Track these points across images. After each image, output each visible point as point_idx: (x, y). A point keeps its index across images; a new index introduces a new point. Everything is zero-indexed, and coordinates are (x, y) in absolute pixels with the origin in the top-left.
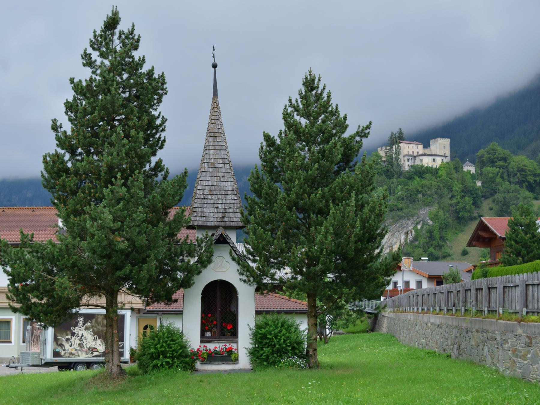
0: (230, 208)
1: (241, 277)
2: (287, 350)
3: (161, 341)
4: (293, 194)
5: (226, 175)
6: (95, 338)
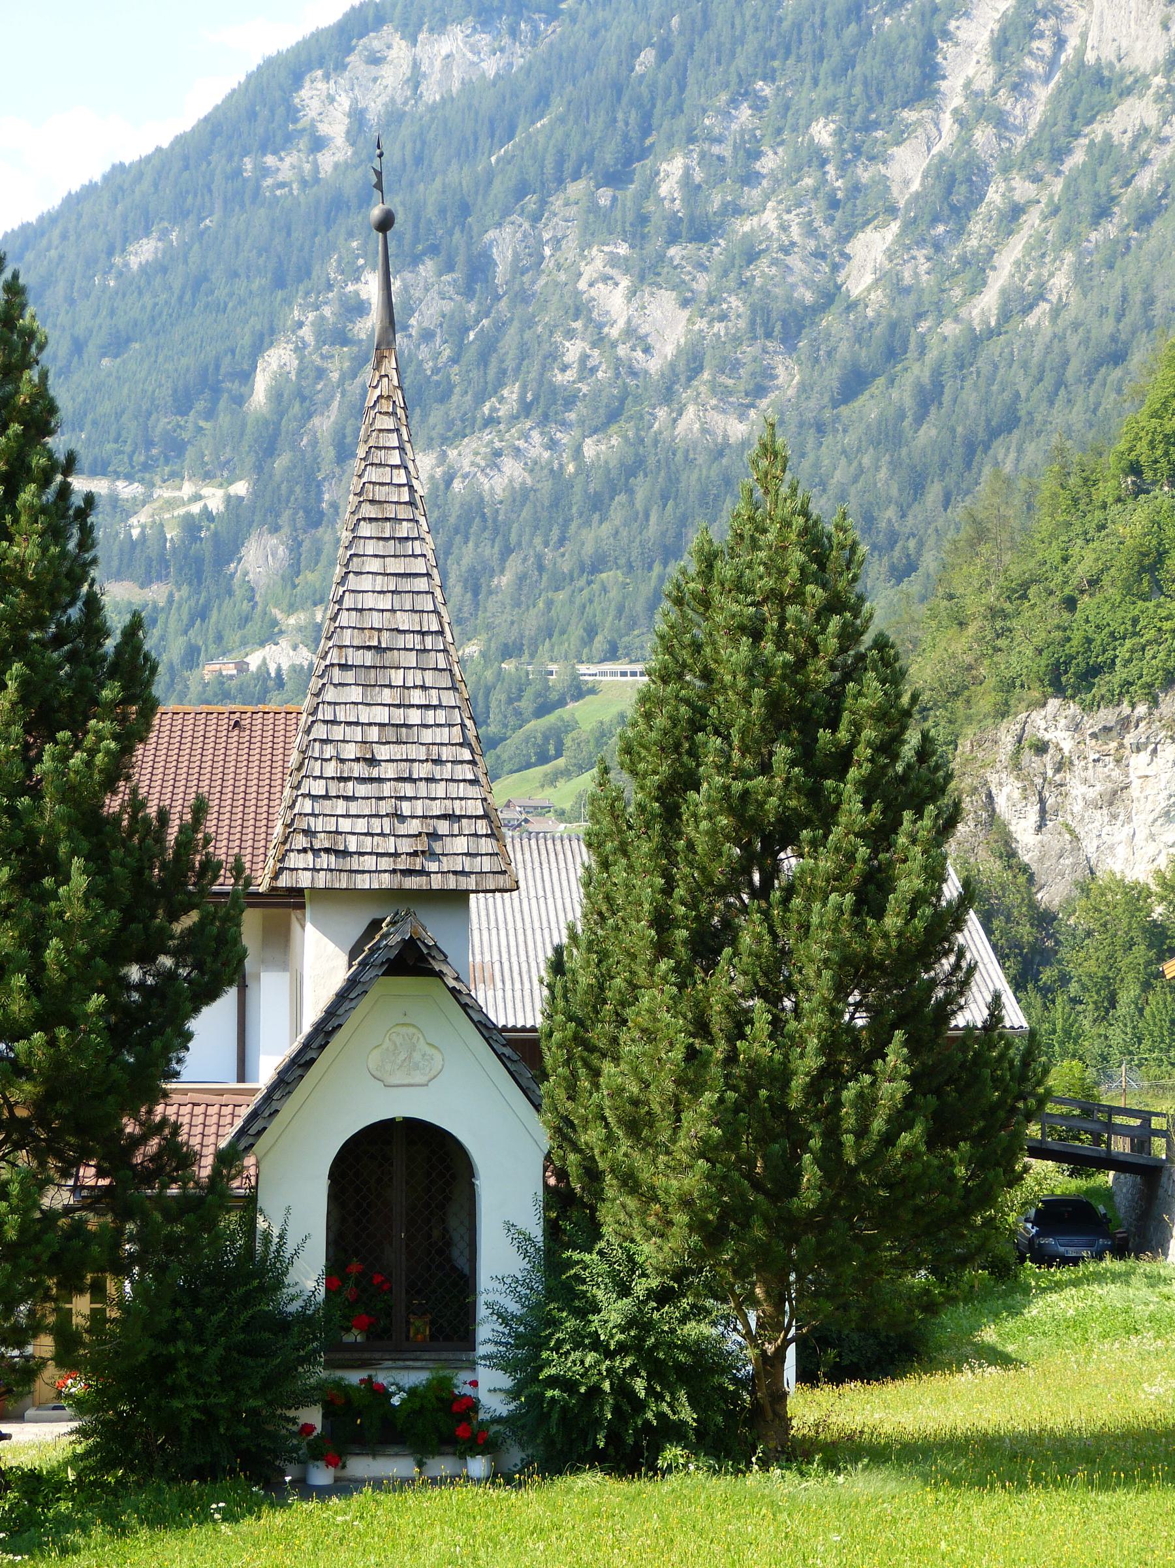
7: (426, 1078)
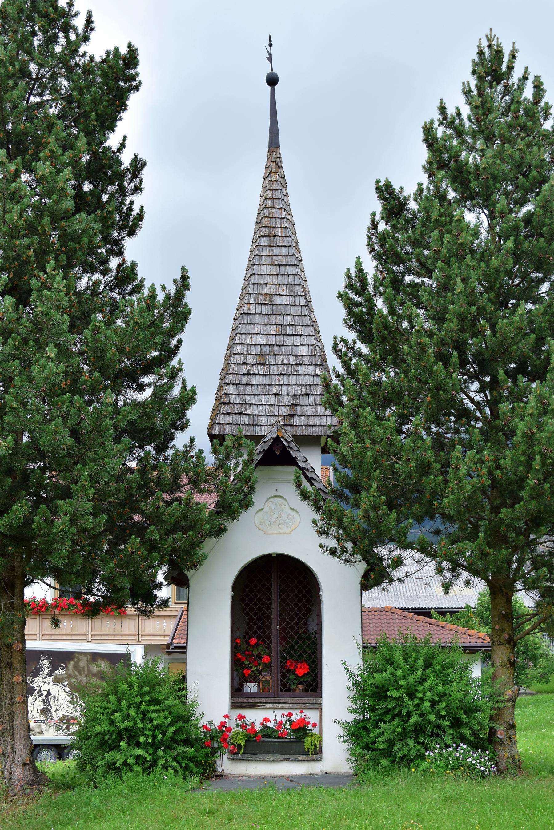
0: (307, 395)
1: (323, 540)
2: (439, 727)
3: (123, 702)
4: (451, 320)
5: (298, 320)
6: (73, 698)
7: (290, 530)
